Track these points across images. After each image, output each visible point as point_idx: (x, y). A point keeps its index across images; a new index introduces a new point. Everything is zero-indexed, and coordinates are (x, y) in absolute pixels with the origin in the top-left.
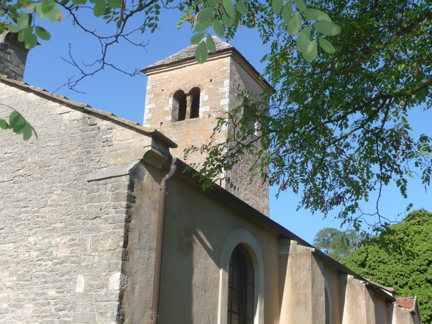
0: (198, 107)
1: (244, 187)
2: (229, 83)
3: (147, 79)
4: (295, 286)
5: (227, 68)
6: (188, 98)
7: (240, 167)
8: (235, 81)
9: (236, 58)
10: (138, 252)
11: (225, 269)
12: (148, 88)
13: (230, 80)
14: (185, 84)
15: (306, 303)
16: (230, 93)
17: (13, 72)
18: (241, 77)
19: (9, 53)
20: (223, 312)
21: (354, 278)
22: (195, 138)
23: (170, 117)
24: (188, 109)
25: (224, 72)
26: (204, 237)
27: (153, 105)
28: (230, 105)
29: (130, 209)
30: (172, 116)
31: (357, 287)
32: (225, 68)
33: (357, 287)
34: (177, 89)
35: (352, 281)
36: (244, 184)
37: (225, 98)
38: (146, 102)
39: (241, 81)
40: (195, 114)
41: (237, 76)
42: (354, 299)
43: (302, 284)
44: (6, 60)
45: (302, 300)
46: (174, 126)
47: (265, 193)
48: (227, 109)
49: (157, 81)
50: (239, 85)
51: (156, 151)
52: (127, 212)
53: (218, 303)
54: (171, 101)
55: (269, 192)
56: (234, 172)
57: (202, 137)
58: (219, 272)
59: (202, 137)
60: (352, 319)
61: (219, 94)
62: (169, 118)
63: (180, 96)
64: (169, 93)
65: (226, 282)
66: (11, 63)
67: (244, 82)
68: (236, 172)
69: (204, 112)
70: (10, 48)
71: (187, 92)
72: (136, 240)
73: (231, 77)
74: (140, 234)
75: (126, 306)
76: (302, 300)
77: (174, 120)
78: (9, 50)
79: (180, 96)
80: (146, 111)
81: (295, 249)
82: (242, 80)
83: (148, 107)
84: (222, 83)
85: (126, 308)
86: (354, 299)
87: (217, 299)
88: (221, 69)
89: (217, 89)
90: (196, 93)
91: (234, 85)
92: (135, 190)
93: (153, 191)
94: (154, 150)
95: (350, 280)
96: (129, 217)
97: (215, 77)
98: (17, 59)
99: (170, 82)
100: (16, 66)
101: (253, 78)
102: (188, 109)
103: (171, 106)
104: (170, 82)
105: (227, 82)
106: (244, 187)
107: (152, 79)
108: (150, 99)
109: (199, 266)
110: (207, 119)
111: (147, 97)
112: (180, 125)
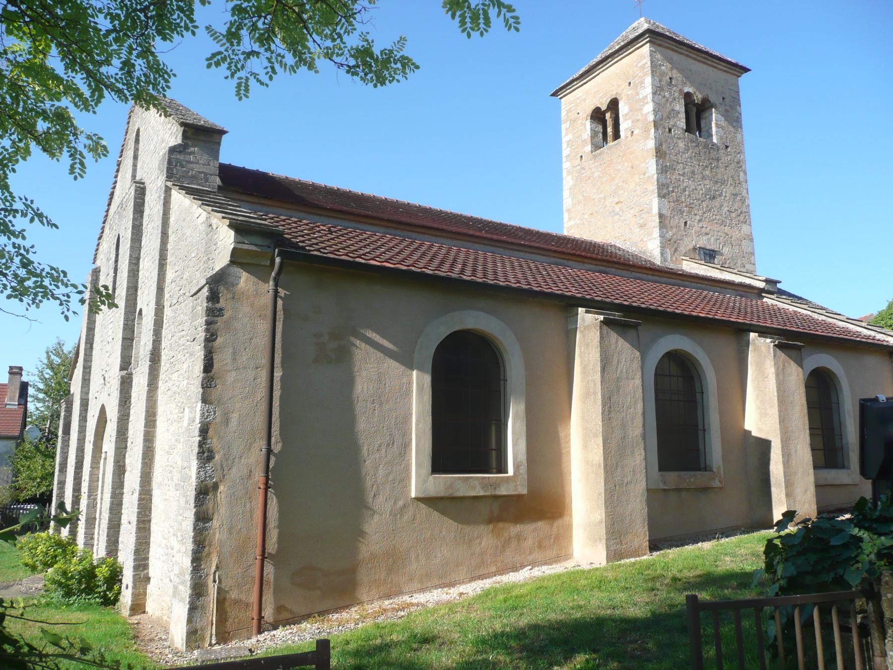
0: (619, 125)
1: (698, 217)
2: (650, 81)
3: (560, 103)
4: (584, 368)
5: (647, 61)
6: (608, 115)
7: (687, 193)
8: (663, 74)
9: (659, 42)
10: (233, 374)
11: (420, 369)
12: (563, 114)
13: (653, 76)
14: (601, 97)
15: (595, 393)
16: (654, 93)
17: (200, 173)
18: (674, 65)
19: (193, 153)
20: (421, 425)
21: (759, 336)
22: (619, 167)
23: (590, 146)
24: (610, 130)
25: (643, 67)
26: (374, 334)
27: (570, 136)
28: (655, 112)
29: (213, 326)
30: (592, 144)
31: (763, 349)
32: (644, 62)
33: (763, 349)
34: (593, 107)
35: (756, 342)
36: (696, 215)
37: (647, 103)
38: (563, 134)
39: (675, 71)
40: (617, 136)
41: (665, 67)
42: (760, 365)
43: (591, 367)
44: (189, 162)
45: (592, 390)
46: (595, 156)
47: (741, 218)
48: (651, 118)
49: (571, 103)
50: (671, 79)
51: (246, 247)
52: (207, 330)
53: (411, 414)
54: (588, 123)
55: (749, 216)
56: (674, 202)
57: (626, 164)
58: (411, 375)
59: (626, 164)
60: (757, 396)
61: (640, 100)
62: (589, 148)
63: (598, 116)
64: (585, 116)
65: (426, 385)
66: (197, 163)
67: (681, 71)
68: (678, 201)
69: (626, 130)
70: (192, 146)
71: (604, 108)
72: (229, 361)
73: (652, 72)
74: (234, 353)
75: (215, 440)
76: (592, 390)
77: (596, 147)
78: (192, 149)
79: (598, 116)
80: (564, 145)
81: (583, 320)
82: (677, 69)
83: (565, 140)
84: (642, 83)
85: (214, 442)
86: (760, 365)
87: (410, 408)
88: (639, 65)
89: (638, 94)
90: (614, 104)
91: (660, 81)
92: (221, 300)
93: (257, 294)
94: (240, 246)
95: (753, 340)
96: (212, 335)
97: (634, 77)
98: (206, 157)
99: (585, 99)
100: (204, 165)
101: (699, 61)
102: (610, 130)
103: (589, 132)
104: (585, 99)
105: (648, 80)
106: (698, 217)
107: (567, 102)
108: (567, 129)
109: (364, 373)
110: (630, 138)
111: (564, 127)
112: (600, 154)
